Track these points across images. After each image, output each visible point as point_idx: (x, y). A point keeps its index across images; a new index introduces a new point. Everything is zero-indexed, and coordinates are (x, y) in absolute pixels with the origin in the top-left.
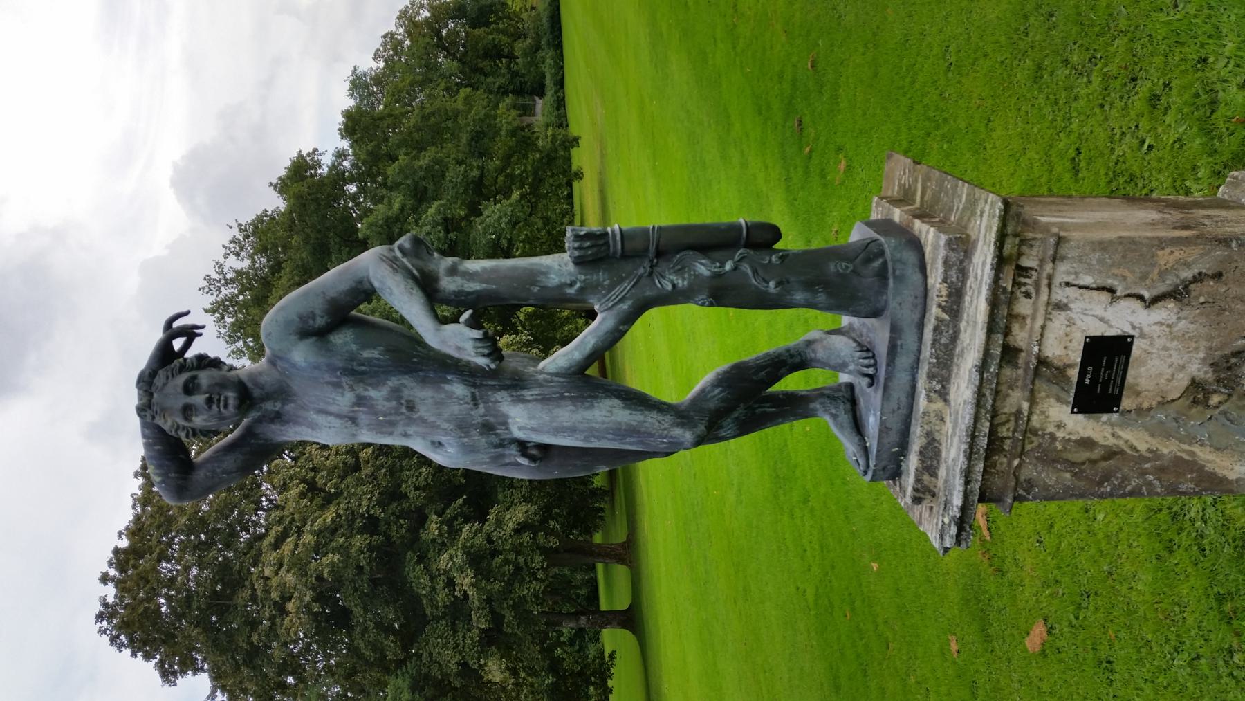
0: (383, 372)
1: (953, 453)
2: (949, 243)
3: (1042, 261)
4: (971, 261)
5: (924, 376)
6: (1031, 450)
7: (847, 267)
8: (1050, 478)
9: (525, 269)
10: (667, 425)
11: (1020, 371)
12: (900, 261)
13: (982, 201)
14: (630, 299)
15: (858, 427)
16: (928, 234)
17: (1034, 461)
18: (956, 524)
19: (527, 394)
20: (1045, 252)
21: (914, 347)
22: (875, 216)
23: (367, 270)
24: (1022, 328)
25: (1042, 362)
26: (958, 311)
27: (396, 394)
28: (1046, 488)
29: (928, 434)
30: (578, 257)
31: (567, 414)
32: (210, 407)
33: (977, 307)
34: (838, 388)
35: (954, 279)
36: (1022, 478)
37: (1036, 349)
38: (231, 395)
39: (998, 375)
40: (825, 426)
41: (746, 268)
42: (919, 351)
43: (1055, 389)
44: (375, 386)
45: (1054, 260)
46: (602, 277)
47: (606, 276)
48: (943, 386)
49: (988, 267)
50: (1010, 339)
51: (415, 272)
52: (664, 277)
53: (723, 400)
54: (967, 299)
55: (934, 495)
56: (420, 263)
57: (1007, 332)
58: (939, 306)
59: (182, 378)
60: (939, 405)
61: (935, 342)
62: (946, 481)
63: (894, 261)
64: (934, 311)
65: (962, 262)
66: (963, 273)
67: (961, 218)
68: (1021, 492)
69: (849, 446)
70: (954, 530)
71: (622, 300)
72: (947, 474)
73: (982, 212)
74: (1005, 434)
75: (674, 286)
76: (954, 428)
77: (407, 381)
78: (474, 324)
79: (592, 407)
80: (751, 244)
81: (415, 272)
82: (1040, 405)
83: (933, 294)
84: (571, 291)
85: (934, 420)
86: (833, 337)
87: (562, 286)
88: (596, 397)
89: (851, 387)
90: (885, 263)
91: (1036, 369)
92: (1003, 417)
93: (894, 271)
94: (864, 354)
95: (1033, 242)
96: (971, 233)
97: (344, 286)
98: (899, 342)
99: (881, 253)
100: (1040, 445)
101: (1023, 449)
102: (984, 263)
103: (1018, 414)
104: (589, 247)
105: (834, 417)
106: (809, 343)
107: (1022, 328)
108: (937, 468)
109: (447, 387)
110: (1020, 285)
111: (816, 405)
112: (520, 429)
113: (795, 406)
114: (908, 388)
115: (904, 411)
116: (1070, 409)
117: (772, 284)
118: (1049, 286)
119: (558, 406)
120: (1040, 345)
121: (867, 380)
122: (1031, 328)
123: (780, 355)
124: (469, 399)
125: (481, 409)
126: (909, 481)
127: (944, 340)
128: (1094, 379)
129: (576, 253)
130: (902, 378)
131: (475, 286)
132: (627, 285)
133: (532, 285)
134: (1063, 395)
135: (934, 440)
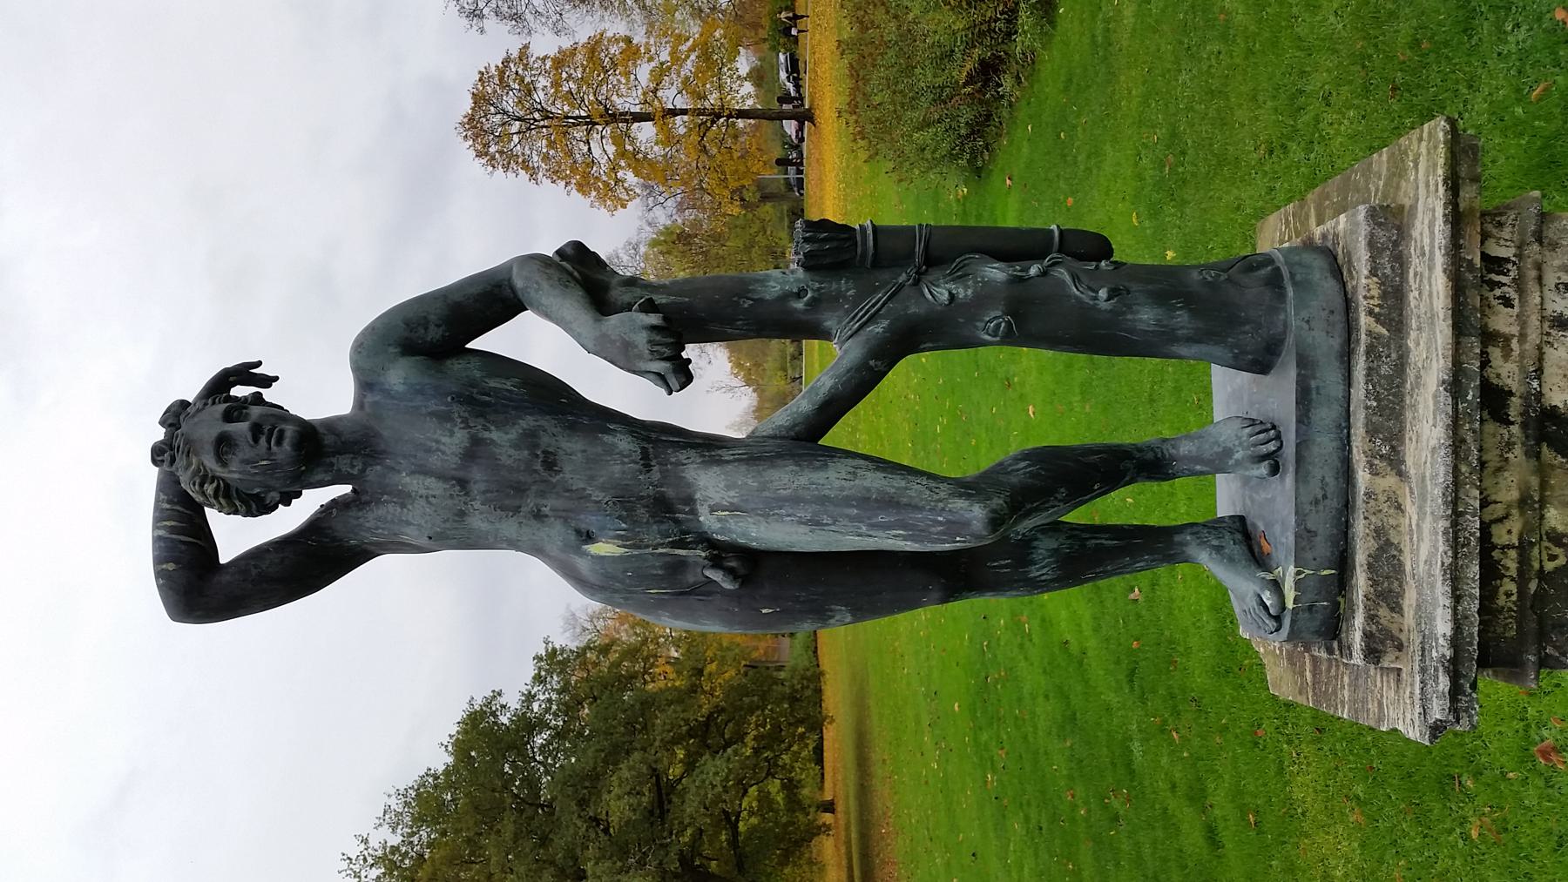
0: (515, 408)
10: (942, 495)
11: (1515, 429)
18: (1447, 671)
20: (1522, 232)
27: (530, 439)
32: (256, 440)
33: (1430, 290)
35: (1388, 271)
41: (1062, 274)
46: (846, 287)
47: (850, 283)
48: (1393, 447)
50: (1490, 372)
55: (1400, 647)
58: (1370, 313)
60: (1390, 481)
61: (1370, 371)
64: (1364, 321)
65: (1396, 244)
66: (1400, 261)
70: (1444, 683)
77: (546, 422)
85: (1385, 507)
87: (786, 297)
98: (1313, 384)
104: (825, 240)
105: (1219, 549)
107: (1507, 355)
108: (1401, 595)
109: (607, 438)
110: (1495, 285)
115: (1334, 503)
117: (1103, 293)
119: (773, 466)
124: (637, 456)
125: (656, 475)
129: (808, 247)
130: (1325, 444)
135: (1388, 543)
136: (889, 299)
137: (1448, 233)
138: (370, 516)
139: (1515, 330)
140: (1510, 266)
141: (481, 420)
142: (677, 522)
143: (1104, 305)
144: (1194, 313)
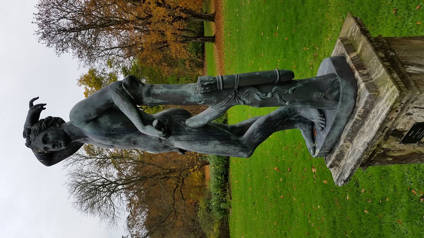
0: (122, 133)
12: (346, 94)
15: (313, 139)
31: (197, 147)
44: (120, 138)
52: (240, 99)
58: (359, 115)
64: (356, 117)
80: (281, 83)
88: (210, 140)
90: (339, 94)
98: (338, 123)
105: (304, 131)
119: (194, 144)
128: (412, 135)
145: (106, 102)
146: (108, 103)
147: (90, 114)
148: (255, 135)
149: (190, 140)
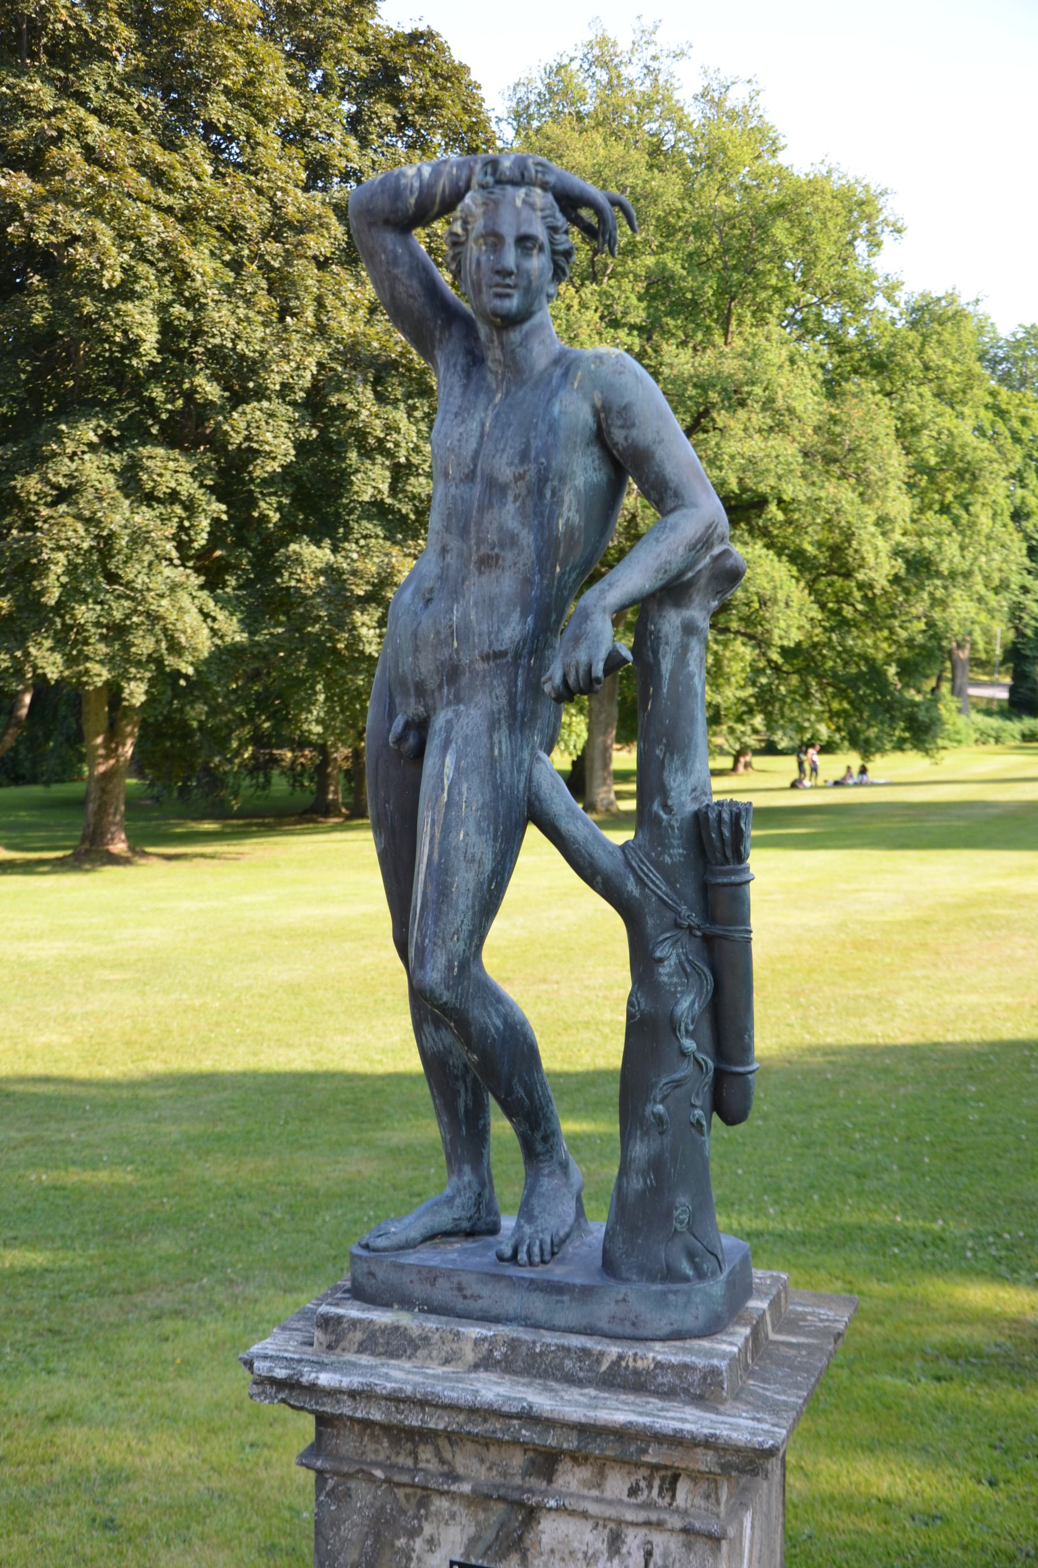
0: (541, 524)
1: (399, 1375)
2: (715, 1372)
3: (685, 1513)
4: (685, 1403)
5: (515, 1335)
6: (396, 1499)
7: (681, 1222)
8: (352, 1528)
9: (690, 739)
11: (518, 1481)
13: (775, 1420)
14: (642, 893)
16: (732, 1343)
17: (378, 1504)
18: (290, 1377)
19: (502, 735)
21: (559, 1320)
22: (759, 1274)
23: (695, 505)
24: (584, 1483)
25: (531, 1514)
26: (612, 1385)
28: (336, 1523)
29: (426, 1339)
30: (707, 818)
33: (618, 1411)
34: (492, 1211)
35: (660, 1379)
36: (352, 1484)
37: (552, 1503)
38: (513, 303)
39: (515, 1442)
40: (435, 1187)
42: (552, 1328)
43: (489, 1535)
44: (522, 512)
45: (686, 1531)
46: (676, 852)
49: (678, 1425)
51: (690, 575)
53: (484, 1032)
54: (631, 1398)
55: (330, 1347)
56: (703, 581)
57: (578, 1458)
58: (621, 1357)
59: (539, 231)
61: (567, 1350)
62: (354, 1365)
63: (688, 1294)
64: (614, 1350)
65: (686, 1391)
66: (669, 1394)
67: (752, 1393)
68: (331, 1483)
69: (401, 1230)
70: (280, 1373)
71: (639, 881)
72: (362, 1366)
73: (758, 1420)
74: (423, 1456)
75: (661, 960)
76: (435, 1376)
78: (614, 662)
79: (480, 832)
80: (720, 1078)
81: (690, 575)
82: (464, 1512)
83: (639, 1349)
84: (656, 806)
85: (447, 1348)
86: (573, 1204)
88: (495, 839)
89: (493, 1230)
90: (686, 1279)
91: (521, 1504)
92: (447, 1455)
93: (676, 1292)
94: (547, 1248)
95: (713, 1500)
96: (728, 1405)
97: (670, 471)
98: (566, 1298)
99: (701, 1275)
100: (404, 1512)
101: (399, 1485)
102: (684, 1420)
103: (454, 1477)
104: (721, 834)
106: (564, 1166)
107: (584, 1483)
108: (373, 1354)
109: (516, 616)
111: (468, 1176)
112: (449, 722)
113: (467, 1139)
114: (494, 1312)
115: (460, 1304)
116: (457, 1558)
117: (660, 1108)
118: (647, 1524)
120: (557, 1509)
121: (508, 1252)
122: (584, 1498)
123: (548, 1120)
124: (498, 647)
125: (480, 666)
126: (353, 1311)
127: (568, 1364)
130: (512, 1302)
131: (666, 665)
132: (663, 889)
133: (667, 746)
134: (481, 1547)
135: (416, 1348)
136: (660, 898)
137: (665, 1431)
138: (456, 379)
139: (608, 1494)
140: (668, 1500)
141: (524, 492)
142: (440, 687)
143: (649, 1109)
144: (641, 1195)
145: (672, 485)
146: (670, 493)
147: (633, 425)
148: (497, 1010)
149: (493, 767)
